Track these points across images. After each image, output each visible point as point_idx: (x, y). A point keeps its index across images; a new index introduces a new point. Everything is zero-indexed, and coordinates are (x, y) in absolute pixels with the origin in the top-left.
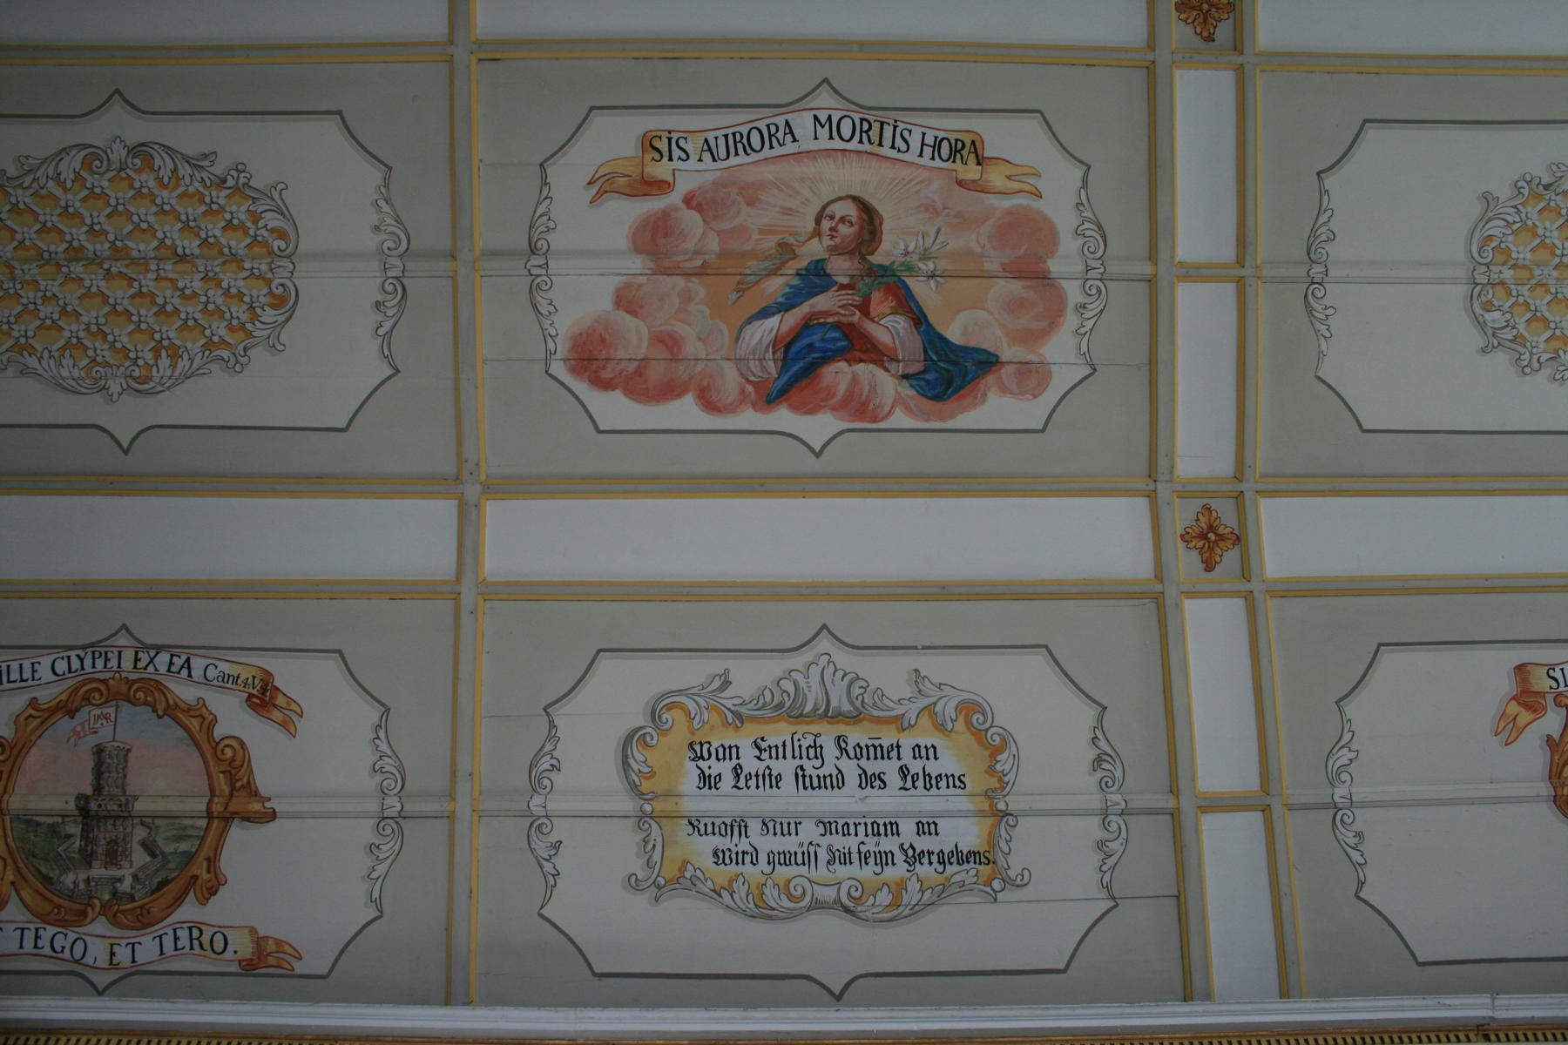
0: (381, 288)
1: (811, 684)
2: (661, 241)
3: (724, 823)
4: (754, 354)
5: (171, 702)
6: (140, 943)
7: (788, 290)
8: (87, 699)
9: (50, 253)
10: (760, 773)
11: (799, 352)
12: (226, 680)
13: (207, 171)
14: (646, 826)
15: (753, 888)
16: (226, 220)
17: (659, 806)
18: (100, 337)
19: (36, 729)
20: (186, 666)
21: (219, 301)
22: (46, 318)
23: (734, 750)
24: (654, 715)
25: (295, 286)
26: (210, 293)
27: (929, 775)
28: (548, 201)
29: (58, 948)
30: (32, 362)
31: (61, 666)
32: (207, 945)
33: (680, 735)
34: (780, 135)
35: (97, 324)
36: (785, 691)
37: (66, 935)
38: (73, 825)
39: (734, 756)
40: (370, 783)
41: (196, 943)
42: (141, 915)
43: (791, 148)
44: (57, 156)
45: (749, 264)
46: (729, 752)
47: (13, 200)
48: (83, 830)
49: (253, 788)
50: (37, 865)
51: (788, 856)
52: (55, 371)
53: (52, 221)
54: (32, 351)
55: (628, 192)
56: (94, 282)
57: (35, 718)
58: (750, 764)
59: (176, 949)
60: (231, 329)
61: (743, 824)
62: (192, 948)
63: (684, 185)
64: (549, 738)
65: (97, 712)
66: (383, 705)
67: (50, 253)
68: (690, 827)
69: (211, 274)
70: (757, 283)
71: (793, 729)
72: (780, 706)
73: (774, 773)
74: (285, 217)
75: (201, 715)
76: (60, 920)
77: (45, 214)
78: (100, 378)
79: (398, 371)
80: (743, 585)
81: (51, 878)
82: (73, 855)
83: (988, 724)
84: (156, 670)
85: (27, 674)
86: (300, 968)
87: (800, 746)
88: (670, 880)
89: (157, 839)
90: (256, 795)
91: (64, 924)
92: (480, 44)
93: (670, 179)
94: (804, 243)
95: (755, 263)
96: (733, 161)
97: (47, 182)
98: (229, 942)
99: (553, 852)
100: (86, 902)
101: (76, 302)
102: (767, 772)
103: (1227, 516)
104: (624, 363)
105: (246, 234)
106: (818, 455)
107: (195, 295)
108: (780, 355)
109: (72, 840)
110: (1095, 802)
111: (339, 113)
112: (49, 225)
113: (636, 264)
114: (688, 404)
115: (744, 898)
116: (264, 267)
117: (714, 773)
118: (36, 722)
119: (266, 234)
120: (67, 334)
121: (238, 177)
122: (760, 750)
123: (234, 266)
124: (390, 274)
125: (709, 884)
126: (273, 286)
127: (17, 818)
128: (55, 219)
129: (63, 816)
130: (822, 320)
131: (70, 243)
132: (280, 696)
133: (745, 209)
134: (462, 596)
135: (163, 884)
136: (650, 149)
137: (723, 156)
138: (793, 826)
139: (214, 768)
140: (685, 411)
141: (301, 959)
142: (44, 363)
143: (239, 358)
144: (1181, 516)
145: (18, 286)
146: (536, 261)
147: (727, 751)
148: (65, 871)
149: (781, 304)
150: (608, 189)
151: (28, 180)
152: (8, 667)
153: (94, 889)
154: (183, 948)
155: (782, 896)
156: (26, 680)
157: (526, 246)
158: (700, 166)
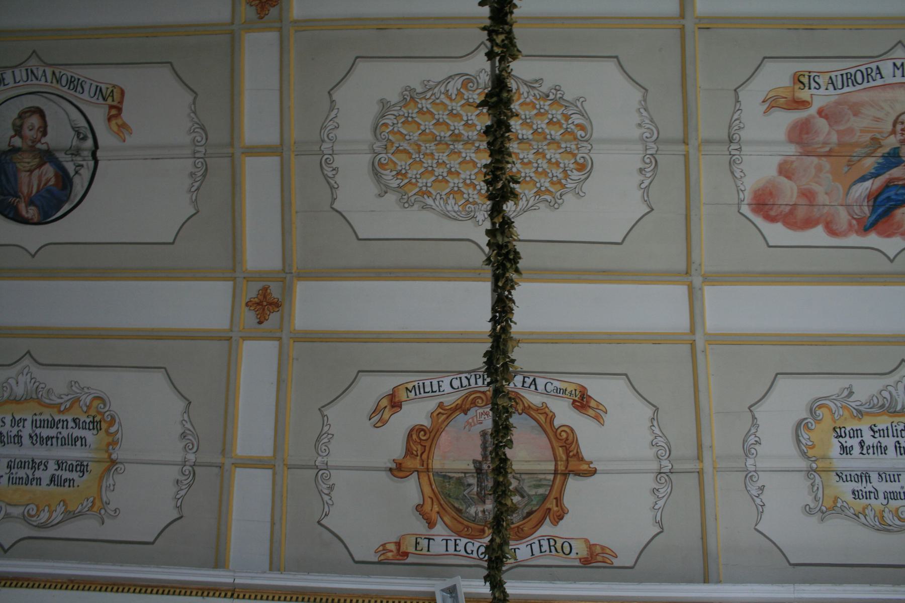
1: (899, 394)
2: (805, 136)
3: (856, 474)
4: (856, 202)
5: (526, 405)
6: (519, 549)
7: (876, 165)
8: (474, 403)
9: (441, 137)
10: (875, 445)
11: (882, 201)
12: (558, 392)
13: (538, 90)
14: (812, 476)
15: (877, 513)
16: (549, 119)
17: (821, 464)
18: (472, 187)
19: (444, 421)
20: (533, 383)
21: (545, 166)
22: (439, 175)
23: (859, 432)
24: (812, 411)
25: (591, 159)
26: (539, 162)
28: (740, 111)
29: (469, 551)
30: (430, 201)
31: (456, 383)
32: (559, 549)
33: (828, 423)
34: (873, 74)
35: (470, 179)
36: (885, 398)
37: (473, 544)
38: (471, 478)
39: (859, 435)
40: (650, 453)
41: (553, 548)
42: (518, 532)
43: (879, 82)
45: (856, 150)
46: (856, 433)
47: (420, 106)
48: (478, 481)
49: (580, 456)
50: (452, 502)
51: (895, 494)
52: (444, 207)
53: (443, 118)
54: (429, 194)
55: (785, 107)
56: (468, 154)
57: (443, 414)
58: (869, 440)
59: (541, 552)
60: (552, 183)
61: (867, 475)
62: (550, 551)
63: (817, 104)
64: (753, 425)
65: (481, 411)
67: (441, 137)
68: (837, 477)
69: (540, 151)
70: (859, 161)
71: (891, 419)
72: (883, 406)
73: (883, 445)
74: (585, 117)
75: (545, 413)
76: (469, 535)
78: (471, 211)
79: (652, 210)
80: (854, 336)
81: (461, 510)
82: (472, 496)
84: (515, 386)
85: (435, 388)
86: (616, 562)
87: (896, 430)
88: (829, 508)
89: (524, 487)
90: (582, 460)
91: (471, 537)
92: (700, 19)
93: (809, 99)
94: (886, 138)
95: (860, 149)
96: (846, 90)
97: (440, 95)
98: (573, 547)
99: (761, 492)
100: (484, 524)
101: (457, 166)
102: (879, 444)
103: (275, 292)
104: (782, 207)
105: (561, 127)
106: (892, 261)
107: (530, 162)
108: (871, 203)
109: (472, 487)
110: (179, 458)
111: (616, 57)
112: (441, 120)
113: (792, 149)
114: (819, 230)
115: (873, 518)
116: (573, 147)
117: (848, 445)
118: (443, 417)
119: (573, 127)
120: (451, 185)
121: (556, 94)
122: (874, 432)
123: (555, 146)
124: (648, 152)
125: (852, 510)
126: (578, 158)
127: (437, 474)
128: (445, 117)
129: (465, 473)
130: (896, 183)
131: (453, 131)
132: (592, 401)
133: (853, 119)
134: (697, 341)
135: (529, 514)
136: (798, 82)
137: (840, 87)
138: (896, 477)
139: (555, 444)
140: (817, 235)
141: (617, 557)
142: (437, 202)
143: (557, 200)
144: (252, 291)
145: (422, 156)
146: (733, 146)
147: (855, 432)
148: (469, 506)
149: (872, 173)
150: (774, 105)
151: (429, 95)
152: (424, 383)
153: (488, 516)
154: (545, 551)
155: (895, 518)
157: (727, 138)
158: (827, 93)
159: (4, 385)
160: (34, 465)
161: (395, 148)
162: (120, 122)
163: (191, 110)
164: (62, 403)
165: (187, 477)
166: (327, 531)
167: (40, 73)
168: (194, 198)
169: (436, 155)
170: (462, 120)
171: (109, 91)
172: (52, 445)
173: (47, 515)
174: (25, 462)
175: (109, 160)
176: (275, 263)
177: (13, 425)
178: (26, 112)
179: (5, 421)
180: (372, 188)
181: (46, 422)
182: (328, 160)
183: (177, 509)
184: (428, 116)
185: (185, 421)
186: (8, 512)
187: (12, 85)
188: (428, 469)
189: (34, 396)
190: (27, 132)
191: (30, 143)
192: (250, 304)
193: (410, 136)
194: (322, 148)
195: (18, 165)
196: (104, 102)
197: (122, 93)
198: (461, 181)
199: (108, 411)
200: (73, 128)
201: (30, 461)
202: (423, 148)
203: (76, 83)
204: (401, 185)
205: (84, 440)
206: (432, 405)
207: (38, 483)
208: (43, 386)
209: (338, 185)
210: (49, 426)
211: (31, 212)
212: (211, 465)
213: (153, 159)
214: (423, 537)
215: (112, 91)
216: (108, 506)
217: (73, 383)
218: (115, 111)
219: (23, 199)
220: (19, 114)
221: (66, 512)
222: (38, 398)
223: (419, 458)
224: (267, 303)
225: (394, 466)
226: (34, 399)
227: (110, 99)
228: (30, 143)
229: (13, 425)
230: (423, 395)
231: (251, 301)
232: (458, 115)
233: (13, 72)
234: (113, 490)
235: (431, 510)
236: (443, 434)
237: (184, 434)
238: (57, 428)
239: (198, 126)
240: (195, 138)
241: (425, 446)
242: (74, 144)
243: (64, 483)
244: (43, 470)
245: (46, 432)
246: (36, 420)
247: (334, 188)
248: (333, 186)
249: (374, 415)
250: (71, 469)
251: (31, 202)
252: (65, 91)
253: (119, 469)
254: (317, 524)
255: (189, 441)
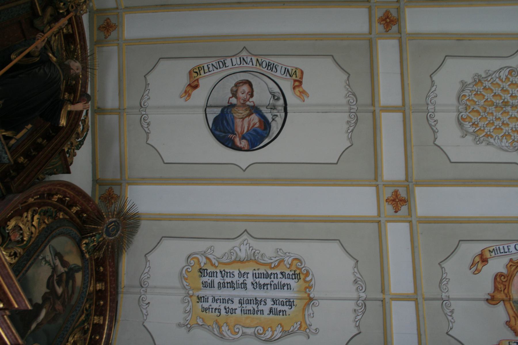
0: (349, 116)
9: (497, 104)
27: (261, 284)
30: (492, 140)
44: (499, 70)
47: (484, 85)
52: (500, 144)
54: (492, 137)
56: (513, 114)
66: (356, 259)
77: (495, 90)
83: (303, 266)
85: (506, 250)
101: (507, 120)
103: (403, 193)
110: (355, 295)
112: (497, 93)
118: (513, 268)
120: (504, 131)
128: (499, 92)
142: (496, 141)
144: (388, 193)
145: (486, 114)
152: (499, 247)
156: (507, 252)
159: (232, 251)
160: (257, 302)
161: (471, 109)
162: (301, 90)
163: (347, 84)
164: (272, 263)
165: (360, 308)
166: (453, 339)
167: (249, 60)
168: (350, 136)
169: (495, 114)
170: (509, 93)
171: (293, 71)
172: (267, 289)
173: (271, 333)
174: (251, 300)
175: (295, 112)
176: (400, 176)
177: (240, 276)
178: (240, 83)
179: (234, 274)
180: (458, 133)
181: (262, 275)
182: (431, 116)
183: (357, 328)
184: (489, 91)
185: (356, 272)
186: (244, 331)
187: (231, 66)
188: (510, 299)
189: (253, 258)
190: (240, 95)
191: (242, 102)
192: (388, 200)
193: (479, 102)
194: (429, 108)
195: (235, 115)
196: (291, 78)
197: (302, 72)
198: (510, 129)
199: (303, 267)
200: (270, 93)
201: (254, 299)
202: (488, 110)
203: (272, 66)
204: (475, 130)
205: (289, 286)
206: (505, 260)
207: (262, 313)
208: (258, 252)
209: (438, 130)
210: (265, 277)
211: (244, 144)
212: (376, 300)
213: (323, 112)
214: (513, 341)
215: (296, 71)
216: (312, 327)
217: (278, 250)
218: (298, 83)
219: (238, 136)
220: (235, 84)
221: (283, 331)
222: (255, 260)
223: (502, 292)
224: (399, 200)
225: (489, 297)
226: (253, 260)
227: (294, 76)
228: (242, 102)
229: (240, 276)
230: (500, 254)
231: (388, 199)
232: (507, 91)
233: (231, 59)
234: (313, 317)
235: (516, 324)
236: (515, 277)
237: (356, 281)
238: (271, 278)
239: (351, 93)
240: (349, 100)
241: (505, 285)
242: (271, 102)
243: (279, 313)
244: (264, 305)
245: (263, 281)
246: (255, 273)
247: (436, 132)
248: (435, 131)
249: (472, 267)
250: (282, 304)
251: (243, 138)
252: (265, 70)
253: (315, 303)
254: (446, 335)
255: (359, 285)
